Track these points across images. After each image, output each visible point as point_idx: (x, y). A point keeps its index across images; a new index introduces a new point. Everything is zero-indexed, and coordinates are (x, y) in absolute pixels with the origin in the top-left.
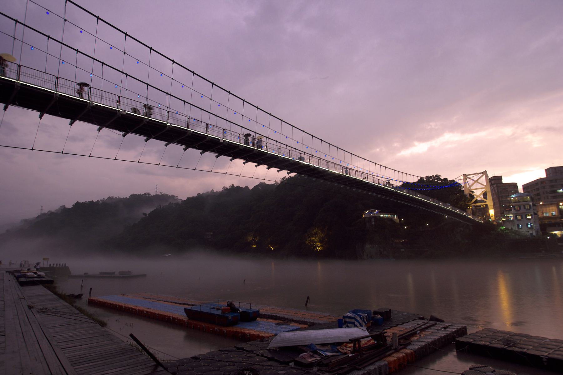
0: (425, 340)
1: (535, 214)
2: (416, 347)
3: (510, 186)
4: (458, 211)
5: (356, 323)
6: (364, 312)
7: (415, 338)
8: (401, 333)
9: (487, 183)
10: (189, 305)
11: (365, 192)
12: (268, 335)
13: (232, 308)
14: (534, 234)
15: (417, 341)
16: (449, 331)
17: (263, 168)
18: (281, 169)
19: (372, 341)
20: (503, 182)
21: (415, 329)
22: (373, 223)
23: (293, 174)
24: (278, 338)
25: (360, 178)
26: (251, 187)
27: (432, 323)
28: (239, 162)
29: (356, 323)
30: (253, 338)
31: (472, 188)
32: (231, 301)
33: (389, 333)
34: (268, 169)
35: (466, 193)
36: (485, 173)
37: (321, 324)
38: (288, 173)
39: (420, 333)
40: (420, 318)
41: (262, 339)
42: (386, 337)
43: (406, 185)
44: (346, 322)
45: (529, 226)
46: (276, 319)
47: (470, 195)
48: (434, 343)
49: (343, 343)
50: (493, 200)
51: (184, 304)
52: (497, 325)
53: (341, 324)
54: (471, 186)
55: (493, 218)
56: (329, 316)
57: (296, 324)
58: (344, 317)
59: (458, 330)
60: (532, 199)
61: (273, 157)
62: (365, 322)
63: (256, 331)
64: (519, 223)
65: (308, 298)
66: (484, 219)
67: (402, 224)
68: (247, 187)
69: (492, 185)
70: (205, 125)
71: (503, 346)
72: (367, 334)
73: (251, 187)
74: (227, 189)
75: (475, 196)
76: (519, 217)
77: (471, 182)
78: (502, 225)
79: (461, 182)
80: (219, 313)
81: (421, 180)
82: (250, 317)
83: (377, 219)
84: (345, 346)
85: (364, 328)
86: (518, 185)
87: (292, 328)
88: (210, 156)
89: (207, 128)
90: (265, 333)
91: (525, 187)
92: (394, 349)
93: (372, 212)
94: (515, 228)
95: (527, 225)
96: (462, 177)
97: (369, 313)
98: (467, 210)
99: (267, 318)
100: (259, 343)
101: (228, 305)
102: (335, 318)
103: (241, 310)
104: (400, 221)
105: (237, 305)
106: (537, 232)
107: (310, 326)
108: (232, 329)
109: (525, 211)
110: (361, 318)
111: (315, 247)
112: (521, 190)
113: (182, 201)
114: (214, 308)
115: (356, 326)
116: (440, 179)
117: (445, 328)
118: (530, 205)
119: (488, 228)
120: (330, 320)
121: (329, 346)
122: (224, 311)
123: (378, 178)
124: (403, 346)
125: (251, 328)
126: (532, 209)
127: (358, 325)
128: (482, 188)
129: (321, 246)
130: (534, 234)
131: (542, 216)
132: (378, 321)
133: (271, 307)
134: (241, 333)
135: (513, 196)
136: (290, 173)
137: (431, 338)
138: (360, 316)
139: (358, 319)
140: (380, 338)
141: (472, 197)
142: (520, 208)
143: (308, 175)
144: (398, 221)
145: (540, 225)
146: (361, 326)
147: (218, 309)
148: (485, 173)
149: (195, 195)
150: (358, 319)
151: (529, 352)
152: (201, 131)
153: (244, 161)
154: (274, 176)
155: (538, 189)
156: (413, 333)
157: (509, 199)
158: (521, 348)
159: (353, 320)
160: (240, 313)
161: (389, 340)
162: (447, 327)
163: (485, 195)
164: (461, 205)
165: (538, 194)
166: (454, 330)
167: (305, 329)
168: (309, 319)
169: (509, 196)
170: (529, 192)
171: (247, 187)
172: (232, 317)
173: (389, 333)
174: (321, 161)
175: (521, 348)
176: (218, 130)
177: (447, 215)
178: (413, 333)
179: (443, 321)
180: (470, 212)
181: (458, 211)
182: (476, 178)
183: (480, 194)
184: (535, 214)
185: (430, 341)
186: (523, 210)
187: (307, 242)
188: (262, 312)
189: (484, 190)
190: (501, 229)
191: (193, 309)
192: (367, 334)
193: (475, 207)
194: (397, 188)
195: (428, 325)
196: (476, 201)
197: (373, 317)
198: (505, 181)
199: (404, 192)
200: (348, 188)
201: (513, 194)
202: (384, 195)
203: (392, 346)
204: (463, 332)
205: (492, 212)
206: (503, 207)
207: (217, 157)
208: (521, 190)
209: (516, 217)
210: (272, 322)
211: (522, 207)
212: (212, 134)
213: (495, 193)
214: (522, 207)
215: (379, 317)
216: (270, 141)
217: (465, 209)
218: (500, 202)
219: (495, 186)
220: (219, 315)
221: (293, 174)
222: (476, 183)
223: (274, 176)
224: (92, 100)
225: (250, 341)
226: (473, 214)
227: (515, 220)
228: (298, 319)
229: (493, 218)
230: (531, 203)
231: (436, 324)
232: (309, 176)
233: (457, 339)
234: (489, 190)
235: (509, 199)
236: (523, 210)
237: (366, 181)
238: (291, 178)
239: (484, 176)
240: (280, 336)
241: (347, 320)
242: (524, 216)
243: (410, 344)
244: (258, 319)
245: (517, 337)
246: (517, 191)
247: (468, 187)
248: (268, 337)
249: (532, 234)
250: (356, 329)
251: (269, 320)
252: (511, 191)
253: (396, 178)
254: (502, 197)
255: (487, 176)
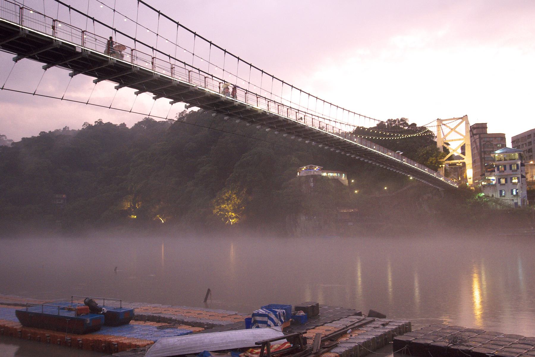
0: (355, 341)
1: (523, 177)
2: (343, 350)
3: (495, 138)
4: (426, 171)
5: (270, 322)
6: (281, 307)
7: (344, 339)
8: (328, 333)
9: (466, 132)
10: (23, 305)
11: (300, 140)
12: (145, 343)
13: (92, 308)
14: (519, 204)
15: (346, 342)
16: (388, 328)
17: (147, 97)
18: (176, 100)
19: (289, 344)
20: (488, 132)
21: (347, 327)
22: (312, 185)
23: (196, 109)
24: (157, 345)
25: (292, 117)
26: (130, 126)
27: (371, 319)
28: (108, 85)
29: (270, 322)
30: (121, 347)
31: (448, 138)
32: (90, 297)
33: (310, 334)
34: (155, 98)
35: (440, 145)
36: (465, 118)
37: (223, 325)
38: (187, 107)
39: (351, 332)
40: (357, 314)
41: (135, 348)
42: (305, 339)
43: (360, 131)
44: (256, 322)
45: (514, 193)
46: (159, 322)
47: (444, 148)
48: (366, 344)
49: (248, 348)
50: (473, 156)
51: (16, 305)
52: (465, 324)
53: (249, 324)
54: (447, 135)
55: (470, 182)
56: (236, 314)
57: (187, 327)
58: (254, 315)
59: (400, 327)
60: (521, 157)
61: (127, 68)
62: (281, 321)
63: (128, 338)
64: (502, 188)
65: (209, 290)
66: (459, 183)
67: (351, 187)
68: (123, 125)
69: (472, 135)
70: (51, 22)
71: (446, 345)
72: (281, 335)
73: (130, 126)
74: (90, 127)
75: (450, 151)
76: (503, 181)
77: (446, 130)
78: (479, 190)
79: (434, 130)
80: (72, 315)
81: (381, 125)
82: (119, 319)
83: (317, 179)
84: (251, 352)
85: (279, 328)
86: (506, 137)
87: (179, 332)
88: (60, 73)
89: (53, 28)
90: (141, 340)
91: (515, 140)
92: (314, 354)
93: (311, 168)
94: (497, 195)
95: (512, 191)
96: (436, 123)
97: (288, 309)
98: (439, 169)
99: (145, 321)
100: (130, 354)
101: (86, 304)
102: (242, 318)
103: (105, 310)
104: (349, 182)
105: (100, 303)
106: (523, 201)
107: (206, 328)
108: (90, 337)
109: (510, 172)
110: (276, 316)
111: (227, 219)
112: (509, 144)
113: (13, 143)
114: (63, 309)
115: (269, 326)
116: (407, 125)
117: (383, 325)
118: (517, 165)
119: (464, 193)
120: (236, 321)
121: (229, 353)
122: (79, 312)
123: (321, 120)
124: (326, 349)
125: (121, 334)
126: (520, 170)
127: (272, 324)
128: (460, 140)
129: (236, 217)
130: (519, 204)
131: (531, 179)
132: (299, 318)
133: (153, 305)
134: (105, 341)
135: (498, 152)
136: (190, 107)
137: (364, 338)
138: (275, 313)
139: (273, 316)
140: (297, 341)
141: (446, 151)
142: (505, 169)
143: (221, 111)
144: (346, 182)
145: (528, 192)
146: (276, 325)
147: (70, 310)
148: (465, 118)
149: (37, 134)
150: (273, 316)
151: (474, 350)
152: (45, 31)
153: (117, 85)
154: (166, 110)
155: (530, 143)
156: (343, 333)
157: (492, 155)
158: (467, 346)
159: (265, 319)
160: (104, 313)
161: (310, 342)
162: (387, 324)
163: (463, 148)
164: (431, 162)
165: (530, 151)
166: (394, 327)
167: (199, 332)
168: (167, 314)
169: (493, 152)
170: (518, 147)
171: (123, 125)
172: (90, 320)
173: (310, 334)
174: (249, 95)
175: (467, 346)
176: (74, 31)
177: (413, 176)
178: (343, 333)
179: (384, 317)
180: (442, 172)
181: (426, 171)
182: (453, 125)
183: (458, 148)
184: (523, 177)
185: (362, 341)
186: (508, 172)
187: (215, 211)
188: (137, 312)
189: (463, 141)
190: (479, 197)
191: (29, 311)
192: (281, 335)
193: (450, 165)
194: (345, 135)
195: (364, 322)
196: (451, 158)
197: (295, 314)
198: (490, 131)
199: (356, 142)
200: (276, 133)
201: (498, 148)
202: (327, 145)
203: (312, 350)
204: (406, 329)
205: (469, 173)
206: (484, 166)
207: (72, 75)
208: (509, 144)
209: (499, 181)
210: (154, 325)
211: (508, 167)
212: (64, 36)
213: (477, 146)
214: (508, 167)
215: (302, 313)
216: (139, 46)
217: (435, 169)
218: (482, 159)
219: (477, 136)
220: (72, 319)
221: (196, 109)
222: (453, 132)
223: (166, 110)
224: (135, 62)
225: (117, 352)
226: (447, 174)
227: (498, 185)
228: (190, 320)
229: (470, 182)
230: (519, 163)
231: (374, 320)
232: (218, 112)
233: (395, 338)
234: (468, 142)
235: (492, 155)
236: (508, 172)
237: (302, 122)
238: (193, 113)
239: (464, 123)
240: (161, 343)
241: (258, 318)
242: (509, 180)
243: (336, 346)
244: (132, 322)
245: (467, 333)
246: (504, 146)
247: (442, 136)
248: (145, 346)
249: (516, 204)
250: (268, 329)
251: (148, 323)
252: (496, 145)
253: (345, 121)
254: (485, 152)
255: (467, 123)
